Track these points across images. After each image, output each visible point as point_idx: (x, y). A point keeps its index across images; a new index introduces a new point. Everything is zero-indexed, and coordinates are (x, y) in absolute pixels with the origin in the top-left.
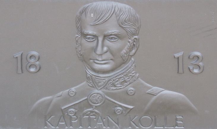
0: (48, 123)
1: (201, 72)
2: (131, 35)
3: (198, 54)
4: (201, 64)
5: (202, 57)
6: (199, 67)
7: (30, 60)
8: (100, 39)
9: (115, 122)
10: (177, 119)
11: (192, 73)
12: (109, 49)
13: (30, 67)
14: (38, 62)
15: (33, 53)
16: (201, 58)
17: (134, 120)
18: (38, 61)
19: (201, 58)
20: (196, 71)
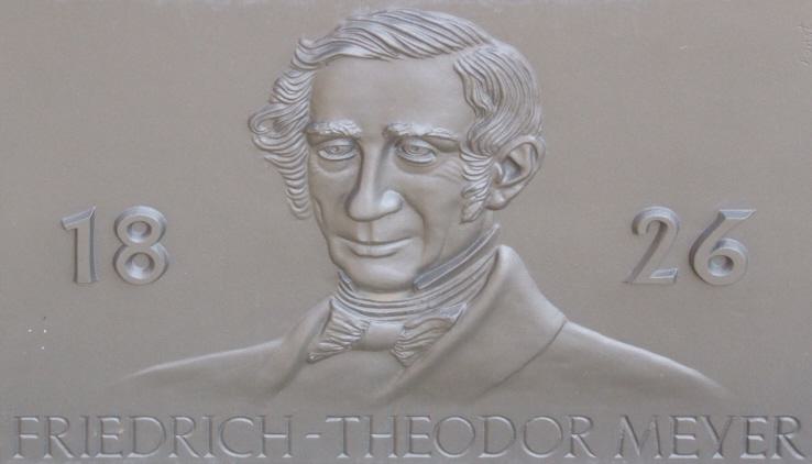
0: (785, 444)
1: (155, 277)
2: (284, 140)
3: (152, 214)
4: (157, 249)
5: (678, 224)
6: (151, 263)
7: (128, 236)
8: (373, 152)
9: (635, 436)
10: (676, 428)
11: (119, 276)
12: (405, 196)
13: (131, 259)
14: (158, 244)
15: (660, 215)
16: (156, 232)
17: (181, 421)
18: (158, 241)
19: (156, 232)
20: (136, 273)
